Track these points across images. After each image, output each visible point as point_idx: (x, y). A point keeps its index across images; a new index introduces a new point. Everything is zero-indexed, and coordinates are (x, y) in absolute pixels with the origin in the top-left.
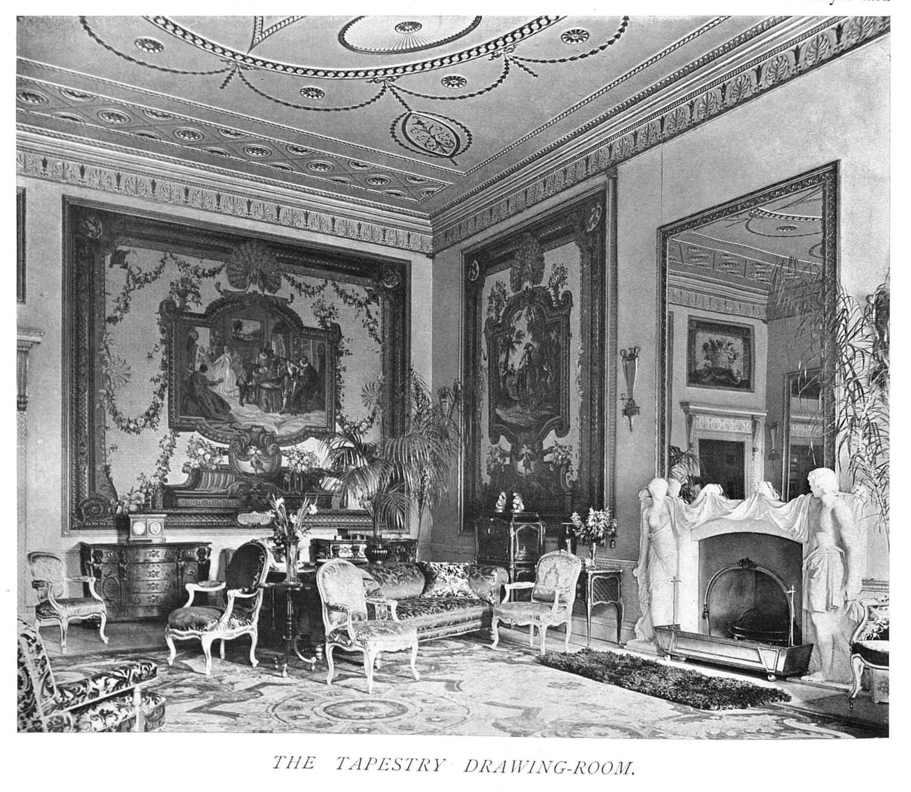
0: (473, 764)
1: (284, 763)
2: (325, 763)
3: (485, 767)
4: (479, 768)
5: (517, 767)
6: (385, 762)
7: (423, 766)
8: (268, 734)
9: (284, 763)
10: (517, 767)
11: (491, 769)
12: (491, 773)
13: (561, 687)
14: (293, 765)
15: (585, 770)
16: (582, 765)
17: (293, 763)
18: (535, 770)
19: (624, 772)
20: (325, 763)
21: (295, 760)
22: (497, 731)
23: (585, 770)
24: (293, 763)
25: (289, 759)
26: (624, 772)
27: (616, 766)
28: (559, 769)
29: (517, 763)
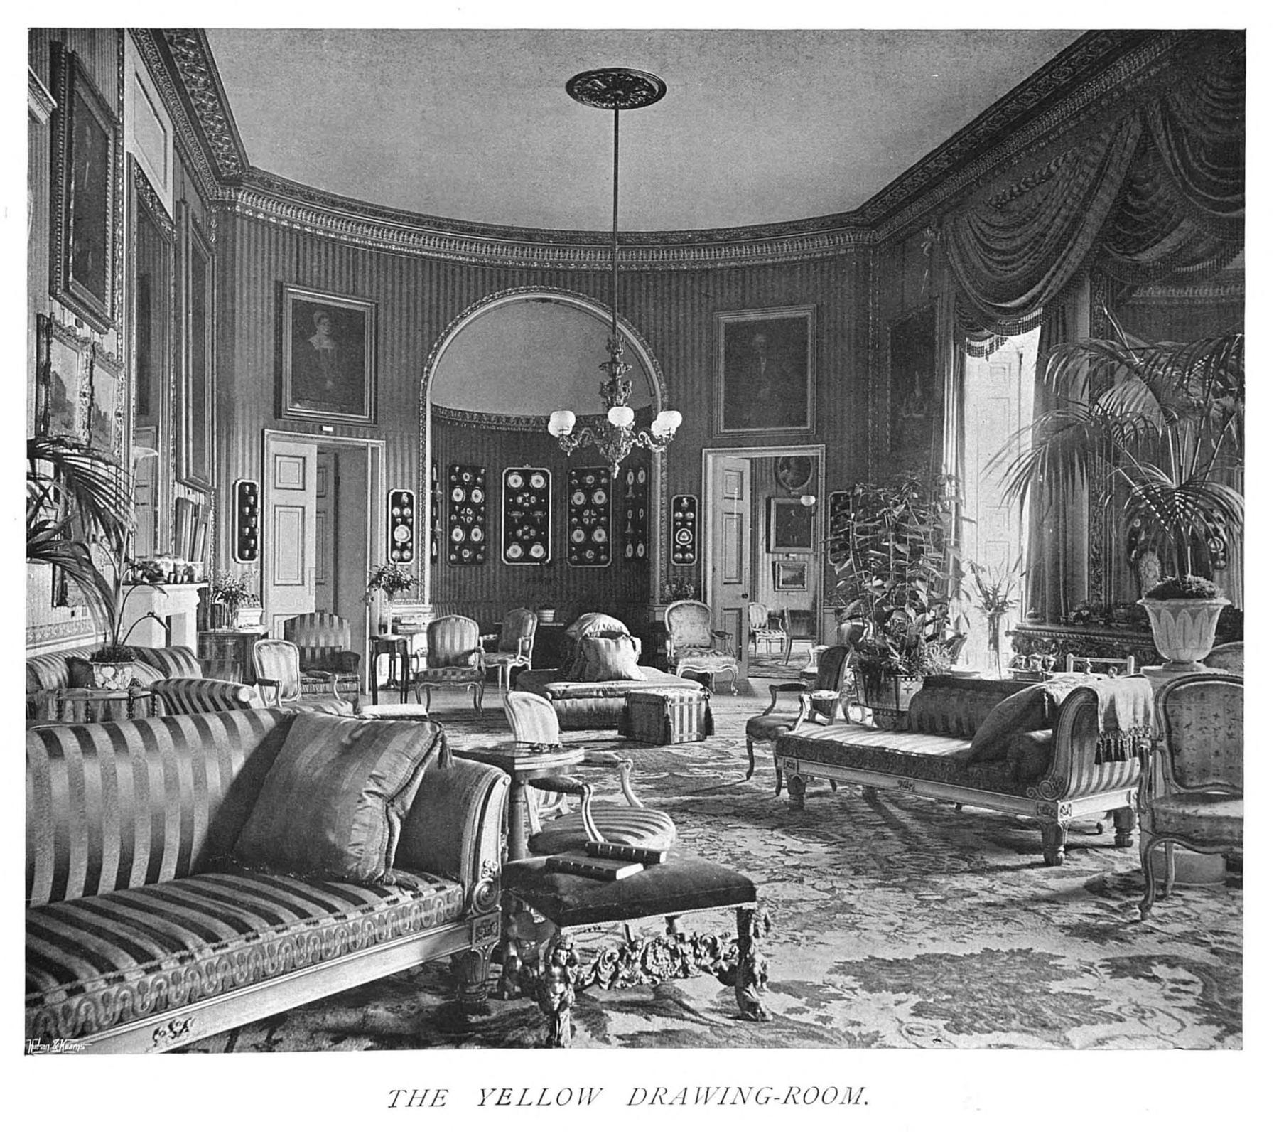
0: (640, 1094)
1: (404, 1099)
2: (462, 1098)
3: (658, 1097)
4: (649, 1098)
5: (704, 1096)
6: (440, 1095)
7: (791, 1098)
8: (837, 1112)
9: (404, 1099)
10: (704, 1096)
11: (666, 1099)
12: (666, 1106)
13: (980, 586)
14: (416, 1101)
15: (799, 1098)
16: (795, 1091)
17: (418, 1099)
18: (728, 1100)
19: (853, 1100)
20: (462, 1098)
21: (420, 1094)
22: (639, 65)
23: (799, 1098)
24: (418, 1099)
25: (723, 1091)
26: (853, 1100)
27: (843, 1093)
28: (762, 1099)
29: (586, 1093)
